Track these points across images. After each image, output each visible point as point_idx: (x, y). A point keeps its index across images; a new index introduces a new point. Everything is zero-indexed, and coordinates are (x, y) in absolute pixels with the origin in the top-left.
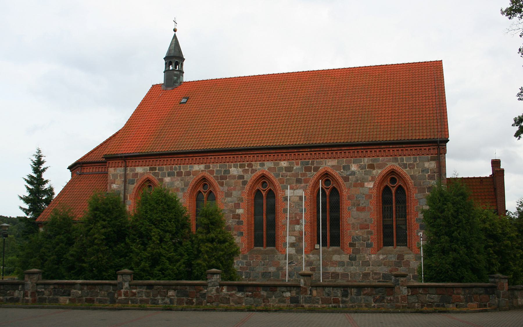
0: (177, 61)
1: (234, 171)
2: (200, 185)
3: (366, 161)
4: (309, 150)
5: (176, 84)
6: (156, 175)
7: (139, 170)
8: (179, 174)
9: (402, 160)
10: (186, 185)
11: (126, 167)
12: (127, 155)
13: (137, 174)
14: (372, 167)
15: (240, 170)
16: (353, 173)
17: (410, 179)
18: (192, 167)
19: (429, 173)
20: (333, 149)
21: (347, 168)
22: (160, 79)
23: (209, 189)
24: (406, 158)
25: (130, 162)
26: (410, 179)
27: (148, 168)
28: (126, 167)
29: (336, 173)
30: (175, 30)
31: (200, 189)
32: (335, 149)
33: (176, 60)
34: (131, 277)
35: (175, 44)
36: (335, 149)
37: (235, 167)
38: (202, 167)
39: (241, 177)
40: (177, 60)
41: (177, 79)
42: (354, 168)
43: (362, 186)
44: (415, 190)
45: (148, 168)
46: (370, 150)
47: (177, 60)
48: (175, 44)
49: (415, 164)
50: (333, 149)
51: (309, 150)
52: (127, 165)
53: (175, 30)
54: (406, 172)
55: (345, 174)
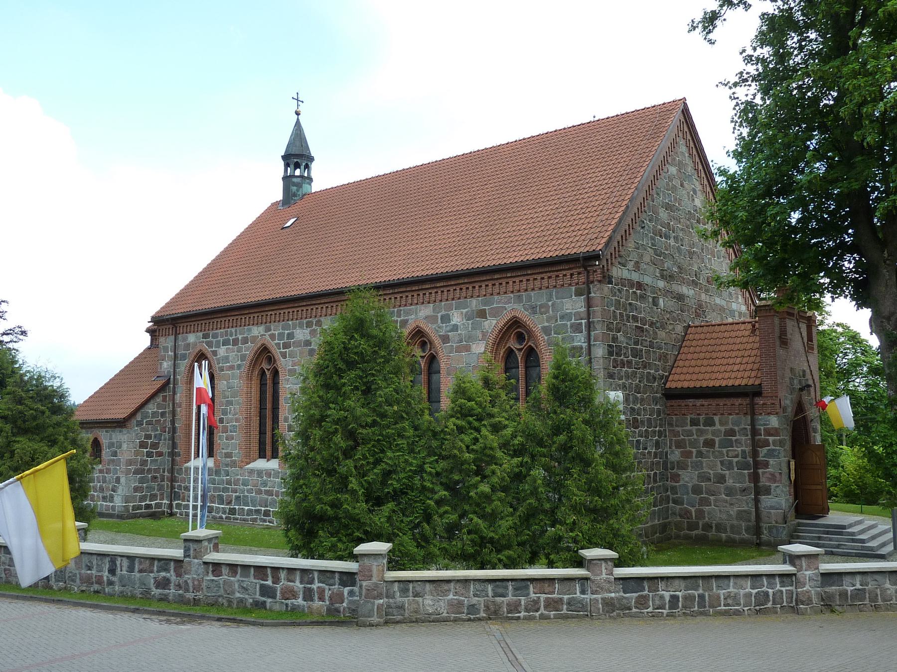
0: (297, 162)
1: (301, 334)
2: (510, 336)
3: (474, 304)
4: (391, 291)
5: (296, 198)
6: (210, 344)
7: (192, 338)
8: (235, 342)
9: (529, 298)
10: (243, 358)
11: (176, 335)
12: (175, 316)
13: (189, 344)
14: (482, 314)
15: (307, 331)
16: (455, 328)
17: (541, 335)
18: (250, 330)
19: (573, 321)
20: (424, 287)
21: (446, 319)
22: (279, 196)
23: (527, 344)
24: (535, 294)
25: (181, 327)
26: (541, 335)
27: (201, 334)
28: (176, 335)
29: (428, 328)
30: (298, 113)
31: (513, 344)
32: (427, 286)
33: (295, 160)
34: (826, 422)
35: (298, 135)
36: (427, 286)
37: (301, 327)
38: (261, 329)
39: (308, 343)
40: (298, 160)
41: (298, 191)
42: (456, 318)
43: (468, 349)
44: (549, 355)
45: (201, 334)
46: (479, 284)
47: (298, 160)
48: (298, 135)
49: (550, 303)
50: (424, 287)
51: (391, 291)
52: (178, 332)
53: (298, 113)
54: (536, 323)
55: (444, 329)
